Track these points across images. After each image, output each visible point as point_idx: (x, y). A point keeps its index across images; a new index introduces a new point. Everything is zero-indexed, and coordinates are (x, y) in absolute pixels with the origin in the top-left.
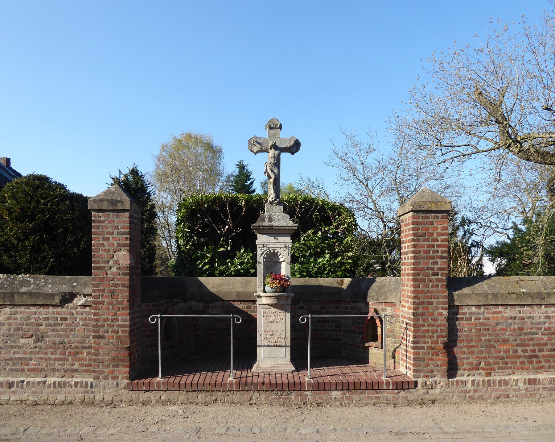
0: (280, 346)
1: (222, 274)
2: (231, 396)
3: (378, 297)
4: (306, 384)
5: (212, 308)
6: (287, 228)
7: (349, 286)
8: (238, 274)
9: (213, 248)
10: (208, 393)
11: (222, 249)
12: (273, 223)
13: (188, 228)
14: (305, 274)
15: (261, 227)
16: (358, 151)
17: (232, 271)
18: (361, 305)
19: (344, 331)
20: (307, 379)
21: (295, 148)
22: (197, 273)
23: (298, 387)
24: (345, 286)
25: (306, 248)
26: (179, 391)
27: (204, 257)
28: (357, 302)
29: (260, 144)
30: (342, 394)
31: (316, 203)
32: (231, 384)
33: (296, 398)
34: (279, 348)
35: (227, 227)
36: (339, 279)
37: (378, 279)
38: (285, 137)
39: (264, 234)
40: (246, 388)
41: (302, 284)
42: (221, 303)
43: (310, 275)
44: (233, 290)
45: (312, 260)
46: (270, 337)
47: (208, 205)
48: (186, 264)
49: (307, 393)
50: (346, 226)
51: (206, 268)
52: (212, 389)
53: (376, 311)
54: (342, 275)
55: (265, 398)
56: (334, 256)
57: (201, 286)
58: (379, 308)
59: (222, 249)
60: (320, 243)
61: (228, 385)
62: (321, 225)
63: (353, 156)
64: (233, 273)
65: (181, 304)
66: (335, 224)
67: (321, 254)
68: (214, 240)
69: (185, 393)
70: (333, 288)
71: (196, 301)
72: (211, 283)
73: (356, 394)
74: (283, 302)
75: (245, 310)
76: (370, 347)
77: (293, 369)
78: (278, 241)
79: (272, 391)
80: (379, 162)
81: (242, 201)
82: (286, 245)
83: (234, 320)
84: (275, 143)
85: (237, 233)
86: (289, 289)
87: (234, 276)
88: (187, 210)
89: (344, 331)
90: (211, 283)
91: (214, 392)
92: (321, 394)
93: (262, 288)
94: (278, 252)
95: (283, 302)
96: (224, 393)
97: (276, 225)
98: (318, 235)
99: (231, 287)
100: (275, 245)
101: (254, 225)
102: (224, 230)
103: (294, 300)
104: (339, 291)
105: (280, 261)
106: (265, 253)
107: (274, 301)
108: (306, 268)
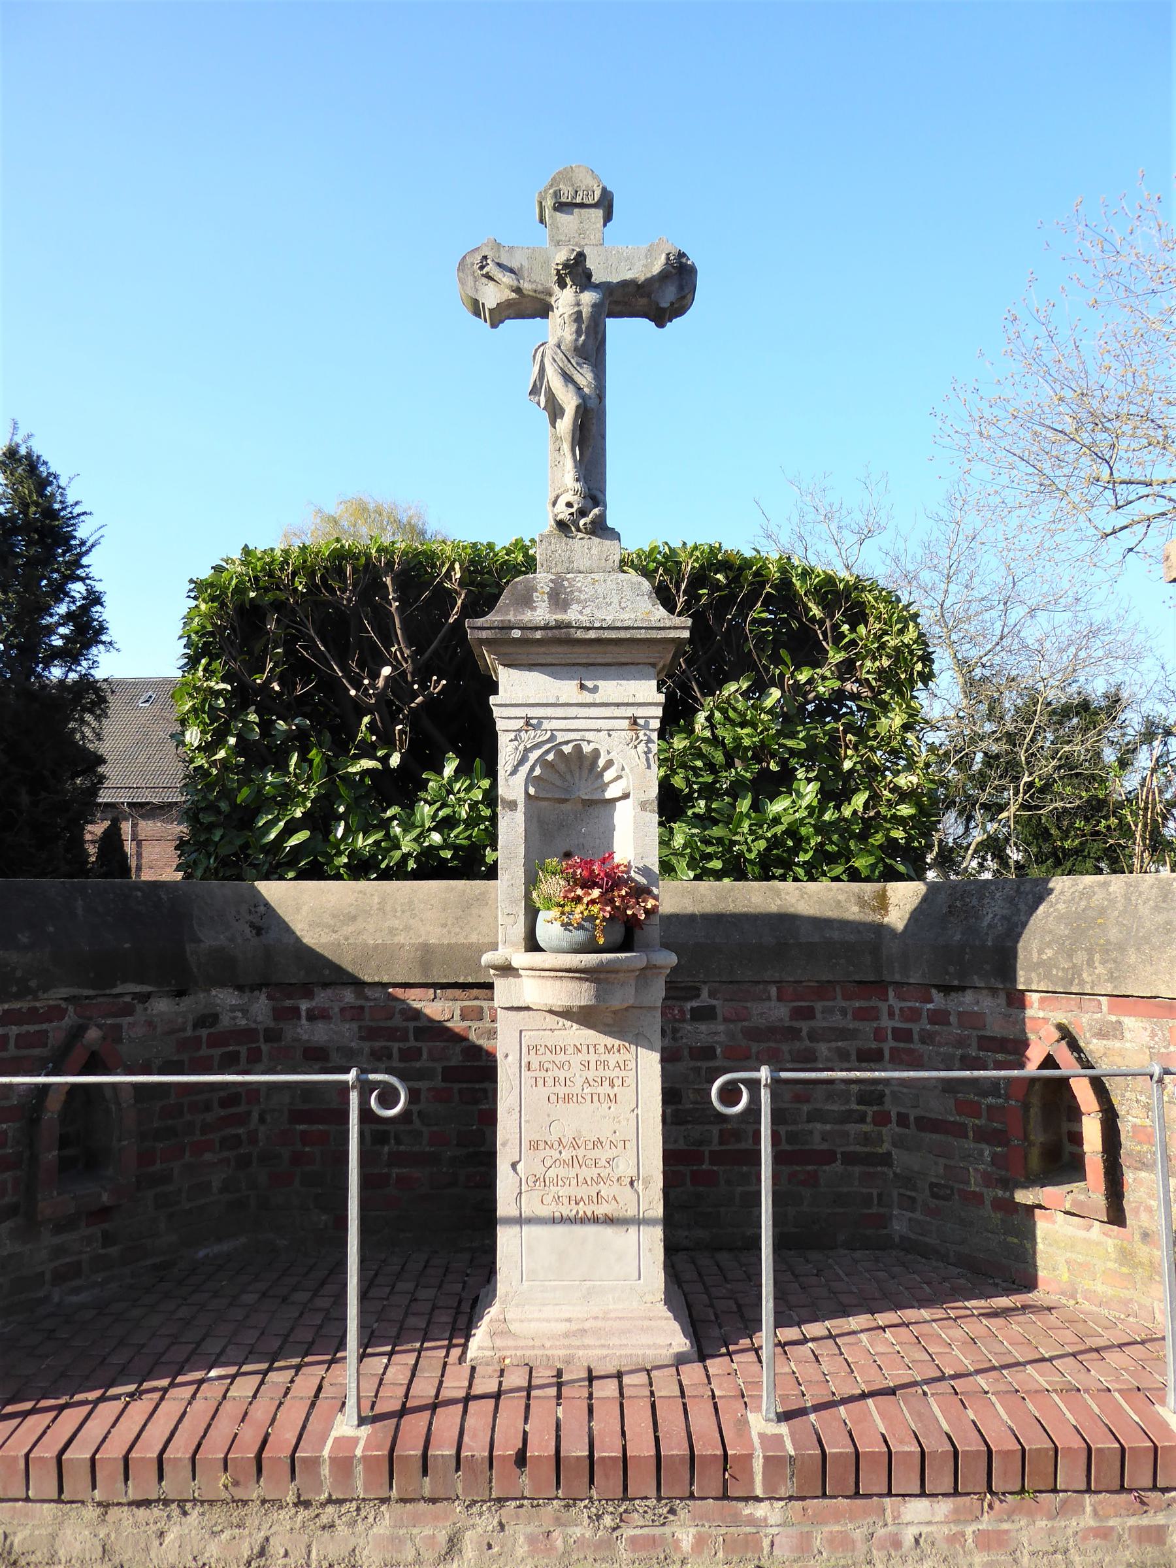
0: (610, 1221)
1: (361, 868)
2: (342, 1530)
3: (1076, 970)
4: (758, 1465)
5: (312, 1017)
6: (642, 634)
7: (917, 916)
8: (430, 867)
9: (327, 760)
10: (217, 1515)
11: (367, 764)
12: (573, 615)
13: (224, 680)
14: (717, 864)
15: (516, 634)
16: (835, 532)
17: (405, 857)
18: (981, 1003)
19: (903, 1120)
20: (760, 1423)
21: (665, 294)
22: (255, 866)
23: (703, 1475)
24: (897, 917)
25: (719, 757)
26: (59, 1501)
27: (288, 796)
28: (963, 989)
29: (512, 271)
30: (956, 1518)
31: (757, 574)
32: (343, 1465)
33: (700, 1542)
34: (608, 1232)
35: (386, 671)
36: (869, 888)
37: (1060, 884)
38: (626, 253)
39: (531, 666)
40: (427, 1486)
41: (708, 908)
42: (349, 996)
43: (736, 869)
44: (401, 939)
45: (744, 805)
46: (563, 1172)
47: (312, 587)
48: (210, 828)
49: (761, 1510)
50: (886, 663)
51: (294, 841)
52: (239, 1493)
53: (1067, 1036)
54: (873, 867)
55: (531, 1540)
56: (835, 791)
57: (266, 920)
58: (1083, 1022)
59: (367, 764)
60: (779, 733)
61: (325, 1471)
62: (777, 660)
63: (820, 546)
64: (412, 865)
65: (162, 1006)
66: (836, 657)
67: (783, 782)
68: (334, 725)
69: (91, 1513)
70: (844, 924)
71: (240, 988)
72: (313, 910)
73: (1030, 1514)
74: (623, 997)
75: (457, 1025)
76: (1040, 1207)
77: (681, 1343)
78: (598, 698)
79: (571, 1502)
80: (896, 560)
81: (452, 568)
82: (634, 721)
83: (369, 1095)
84: (581, 257)
85: (430, 701)
86: (654, 933)
87: (416, 875)
88: (223, 605)
89: (903, 1120)
90: (313, 910)
91: (254, 1507)
92: (837, 1517)
93: (518, 930)
94: (596, 753)
95: (623, 997)
96: (304, 1514)
97: (584, 620)
98: (769, 703)
99: (396, 923)
100: (583, 723)
101: (480, 622)
102: (373, 685)
103: (687, 989)
104: (873, 936)
105: (609, 795)
106: (534, 756)
107: (580, 994)
108: (720, 841)
